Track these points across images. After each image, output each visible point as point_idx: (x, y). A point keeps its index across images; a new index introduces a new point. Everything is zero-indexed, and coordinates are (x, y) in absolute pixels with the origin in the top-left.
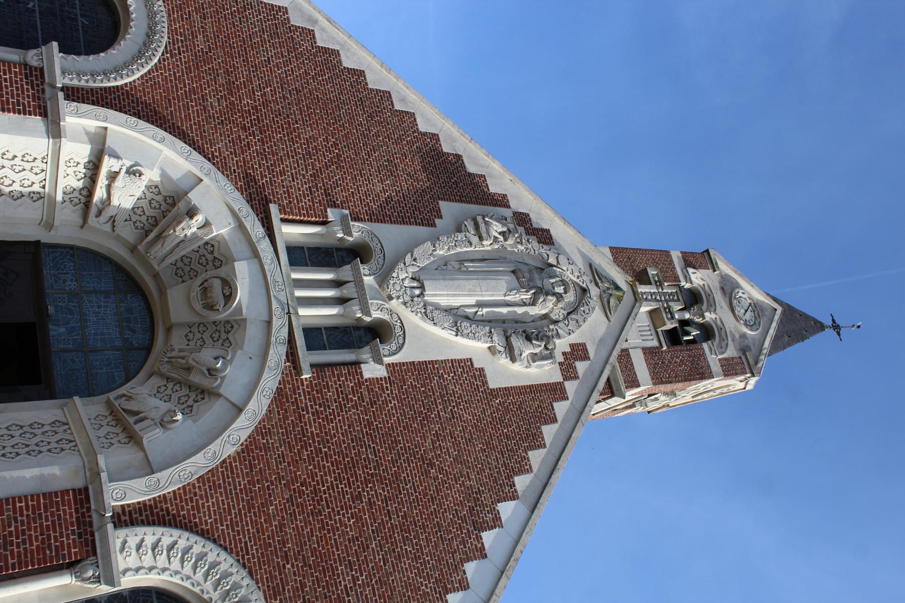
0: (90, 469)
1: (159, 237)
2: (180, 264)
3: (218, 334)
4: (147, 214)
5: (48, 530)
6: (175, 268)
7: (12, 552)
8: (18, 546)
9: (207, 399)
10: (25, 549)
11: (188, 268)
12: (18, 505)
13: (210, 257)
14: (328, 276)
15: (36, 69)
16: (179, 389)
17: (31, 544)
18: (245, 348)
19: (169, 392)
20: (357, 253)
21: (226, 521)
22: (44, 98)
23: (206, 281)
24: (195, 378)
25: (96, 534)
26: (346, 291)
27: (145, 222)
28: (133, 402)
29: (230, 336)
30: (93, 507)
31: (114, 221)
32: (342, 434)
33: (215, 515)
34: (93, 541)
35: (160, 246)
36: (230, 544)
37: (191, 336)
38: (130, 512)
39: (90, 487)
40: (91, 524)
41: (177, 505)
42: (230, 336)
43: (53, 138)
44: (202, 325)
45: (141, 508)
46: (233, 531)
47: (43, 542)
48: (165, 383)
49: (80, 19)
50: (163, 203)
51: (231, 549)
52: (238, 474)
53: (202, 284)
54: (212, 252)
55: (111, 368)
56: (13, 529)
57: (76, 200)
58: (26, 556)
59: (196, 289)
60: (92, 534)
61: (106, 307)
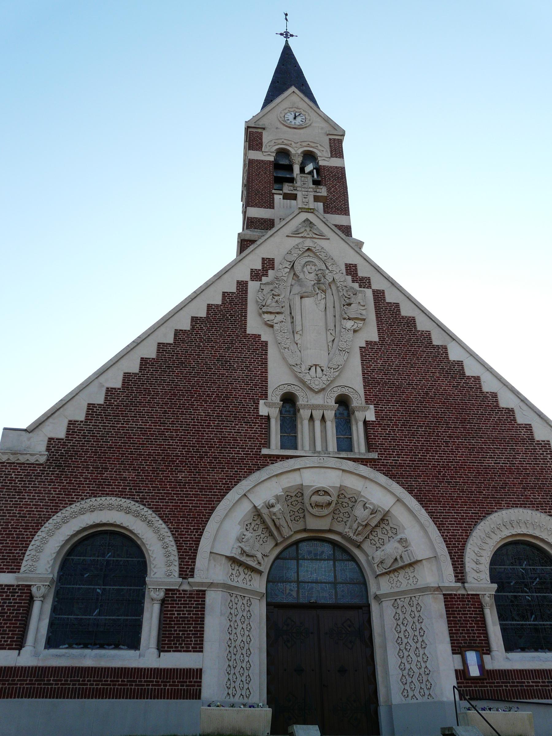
0: (434, 591)
1: (278, 528)
2: (293, 518)
3: (344, 503)
4: (260, 533)
5: (466, 617)
6: (294, 521)
7: (477, 637)
8: (475, 633)
9: (389, 518)
10: (476, 630)
11: (296, 513)
12: (454, 631)
13: (293, 499)
14: (306, 422)
15: (166, 594)
16: (376, 533)
17: (474, 627)
18: (359, 489)
19: (376, 539)
20: (289, 400)
21: (460, 521)
22: (190, 591)
23: (311, 504)
24: (373, 523)
25: (469, 593)
26: (317, 415)
27: (265, 535)
28: (386, 561)
29: (348, 496)
30: (455, 593)
31: (264, 555)
32: (410, 443)
33: (458, 527)
34: (472, 595)
35: (283, 529)
36: (473, 522)
37: (339, 519)
38: (456, 573)
39: (444, 593)
40: (463, 595)
41: (452, 547)
42: (348, 496)
43: (380, 599)
44: (335, 512)
45: (455, 568)
46: (466, 519)
47: (473, 621)
48: (369, 540)
49: (107, 558)
50: (256, 522)
51: (476, 522)
52: (435, 510)
53: (312, 507)
54: (291, 497)
55: (346, 569)
56: (466, 635)
57: (250, 577)
58: (480, 630)
59: (315, 511)
60: (468, 595)
61: (307, 567)
